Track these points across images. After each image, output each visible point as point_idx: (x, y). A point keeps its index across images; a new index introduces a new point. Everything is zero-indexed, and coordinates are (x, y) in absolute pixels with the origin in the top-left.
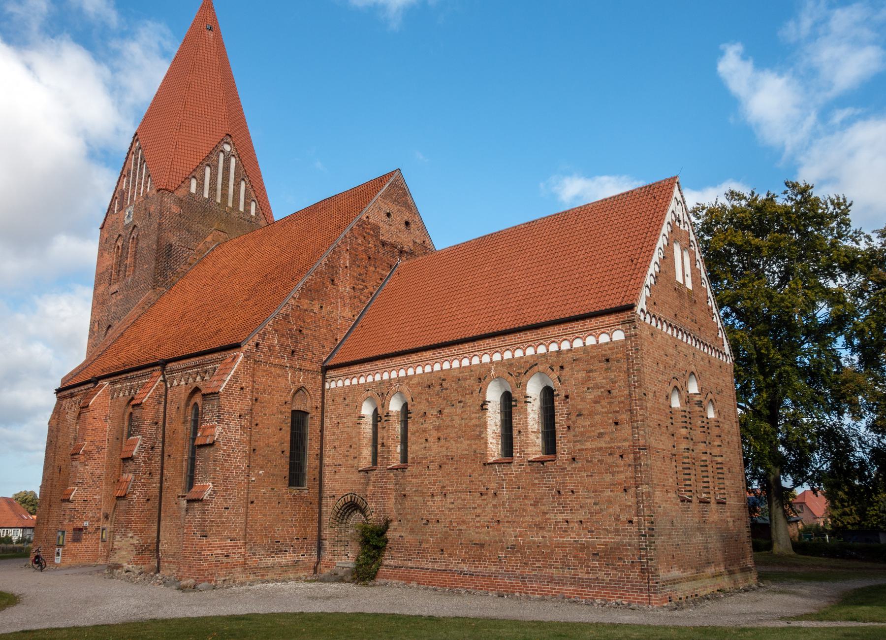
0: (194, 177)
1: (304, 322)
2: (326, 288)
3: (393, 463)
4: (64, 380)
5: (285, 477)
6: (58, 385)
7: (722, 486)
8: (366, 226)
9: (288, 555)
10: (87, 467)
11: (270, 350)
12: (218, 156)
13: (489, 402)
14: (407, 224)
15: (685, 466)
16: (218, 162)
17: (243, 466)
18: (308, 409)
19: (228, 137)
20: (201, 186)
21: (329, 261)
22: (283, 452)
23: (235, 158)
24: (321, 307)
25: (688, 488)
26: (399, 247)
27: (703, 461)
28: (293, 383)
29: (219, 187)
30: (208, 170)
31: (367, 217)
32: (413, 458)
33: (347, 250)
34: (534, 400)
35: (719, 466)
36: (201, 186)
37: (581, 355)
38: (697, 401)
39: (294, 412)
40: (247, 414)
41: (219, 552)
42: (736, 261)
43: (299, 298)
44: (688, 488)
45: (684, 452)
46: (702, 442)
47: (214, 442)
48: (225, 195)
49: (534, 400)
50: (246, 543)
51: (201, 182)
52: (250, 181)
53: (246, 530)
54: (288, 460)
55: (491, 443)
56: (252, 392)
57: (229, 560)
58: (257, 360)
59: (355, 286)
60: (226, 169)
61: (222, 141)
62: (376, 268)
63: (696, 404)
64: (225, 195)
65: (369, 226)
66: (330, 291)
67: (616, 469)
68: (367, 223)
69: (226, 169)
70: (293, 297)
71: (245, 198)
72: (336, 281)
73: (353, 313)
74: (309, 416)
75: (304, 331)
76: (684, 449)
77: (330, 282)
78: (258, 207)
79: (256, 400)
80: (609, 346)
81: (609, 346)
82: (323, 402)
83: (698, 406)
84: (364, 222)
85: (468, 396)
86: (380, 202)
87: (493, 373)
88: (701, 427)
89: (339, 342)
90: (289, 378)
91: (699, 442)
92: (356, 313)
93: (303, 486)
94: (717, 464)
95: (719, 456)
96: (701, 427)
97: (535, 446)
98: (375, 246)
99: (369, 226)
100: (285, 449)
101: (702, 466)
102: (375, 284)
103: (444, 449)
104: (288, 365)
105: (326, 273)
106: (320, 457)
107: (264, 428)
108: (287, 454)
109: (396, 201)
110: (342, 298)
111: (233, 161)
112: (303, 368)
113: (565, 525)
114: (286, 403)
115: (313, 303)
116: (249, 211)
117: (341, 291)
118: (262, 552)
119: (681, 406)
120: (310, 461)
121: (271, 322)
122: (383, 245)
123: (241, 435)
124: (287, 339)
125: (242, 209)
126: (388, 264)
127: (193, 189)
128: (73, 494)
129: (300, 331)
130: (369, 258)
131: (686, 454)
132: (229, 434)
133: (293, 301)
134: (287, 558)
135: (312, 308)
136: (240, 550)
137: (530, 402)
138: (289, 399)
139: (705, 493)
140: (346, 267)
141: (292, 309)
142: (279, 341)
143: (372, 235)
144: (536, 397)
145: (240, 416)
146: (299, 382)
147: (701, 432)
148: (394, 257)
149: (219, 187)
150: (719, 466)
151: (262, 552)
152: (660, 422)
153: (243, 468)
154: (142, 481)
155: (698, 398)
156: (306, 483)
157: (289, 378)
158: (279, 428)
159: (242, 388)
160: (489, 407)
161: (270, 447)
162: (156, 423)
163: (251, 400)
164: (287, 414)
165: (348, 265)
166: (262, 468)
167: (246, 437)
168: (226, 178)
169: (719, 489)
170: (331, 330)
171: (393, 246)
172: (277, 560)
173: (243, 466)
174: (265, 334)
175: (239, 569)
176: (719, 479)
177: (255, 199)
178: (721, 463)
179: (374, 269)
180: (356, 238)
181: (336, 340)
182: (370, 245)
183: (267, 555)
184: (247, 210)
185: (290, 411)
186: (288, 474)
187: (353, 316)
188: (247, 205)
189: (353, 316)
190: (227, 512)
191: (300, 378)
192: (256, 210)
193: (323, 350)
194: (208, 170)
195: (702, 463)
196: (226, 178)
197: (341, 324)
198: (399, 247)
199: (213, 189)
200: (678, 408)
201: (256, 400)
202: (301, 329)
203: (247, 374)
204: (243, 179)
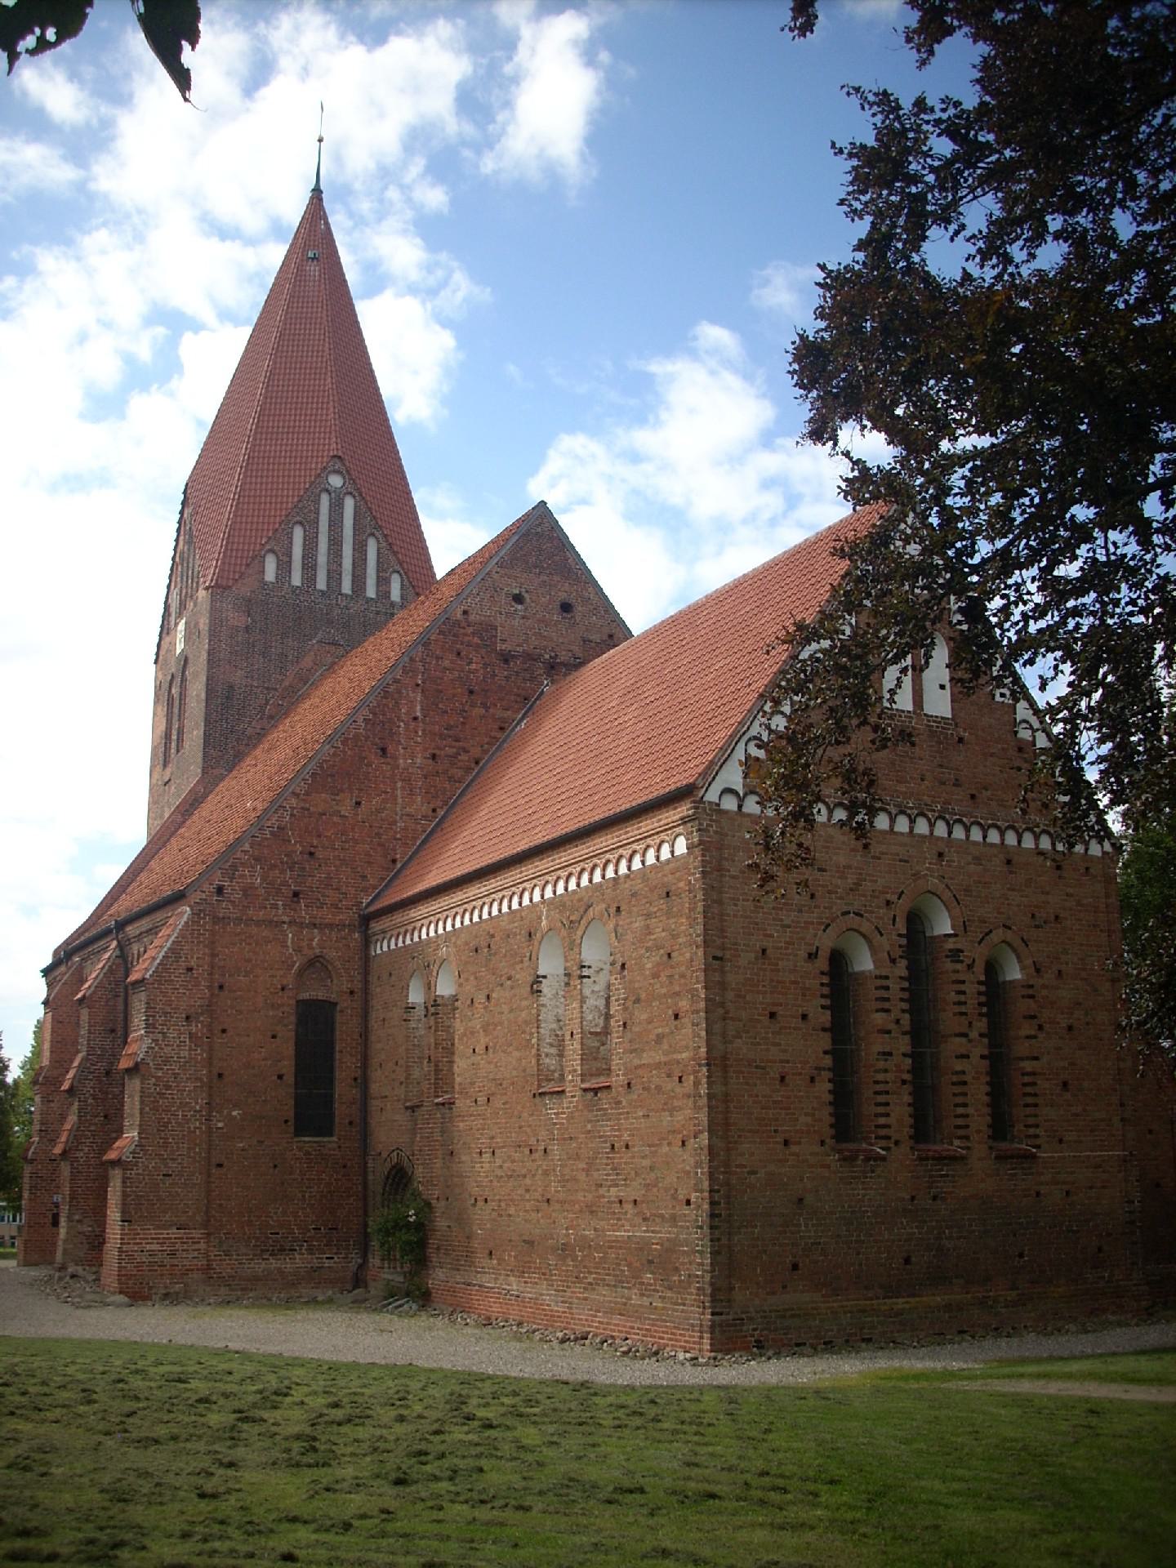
0: (272, 551)
1: (319, 836)
2: (369, 765)
3: (446, 1092)
4: (56, 952)
5: (286, 1121)
6: (48, 960)
7: (1031, 1121)
8: (462, 631)
9: (297, 1256)
10: (52, 1105)
11: (245, 895)
12: (317, 502)
13: (544, 977)
14: (566, 608)
15: (879, 1087)
16: (317, 512)
17: (197, 1103)
18: (333, 997)
19: (336, 460)
20: (284, 567)
21: (375, 714)
22: (280, 1077)
23: (354, 497)
24: (358, 804)
25: (882, 1132)
26: (547, 656)
27: (957, 1073)
28: (298, 950)
29: (322, 559)
30: (298, 534)
31: (465, 612)
32: (460, 1084)
33: (418, 685)
34: (598, 972)
35: (1026, 1079)
36: (284, 567)
37: (638, 885)
38: (950, 950)
39: (301, 1003)
40: (202, 1014)
41: (155, 1247)
42: (1147, 619)
43: (307, 794)
44: (882, 1132)
45: (877, 1060)
46: (957, 1035)
47: (137, 1065)
48: (334, 575)
49: (598, 972)
50: (209, 1234)
51: (286, 559)
52: (386, 536)
53: (207, 1212)
54: (292, 1090)
55: (547, 1055)
56: (211, 974)
57: (175, 1262)
58: (221, 915)
59: (437, 752)
60: (336, 524)
61: (326, 471)
62: (487, 709)
63: (947, 956)
64: (334, 575)
65: (470, 630)
66: (376, 770)
67: (676, 1103)
68: (463, 624)
69: (336, 524)
70: (293, 793)
71: (378, 571)
72: (390, 749)
73: (432, 806)
74: (338, 1008)
75: (319, 854)
76: (879, 1053)
77: (376, 753)
78: (405, 583)
79: (221, 987)
80: (671, 865)
81: (671, 865)
82: (366, 982)
83: (952, 961)
84: (458, 623)
85: (518, 967)
86: (496, 576)
87: (544, 923)
88: (955, 1004)
89: (399, 865)
90: (289, 943)
91: (951, 1036)
92: (439, 803)
93: (332, 1135)
94: (1023, 1074)
95: (1028, 1058)
96: (955, 1004)
97: (595, 1059)
98: (486, 665)
99: (470, 630)
100: (284, 1071)
101: (954, 1084)
102: (486, 740)
103: (492, 1066)
104: (286, 919)
105: (367, 738)
106: (363, 1081)
107: (238, 1035)
108: (290, 1078)
109: (535, 567)
110: (407, 780)
111: (349, 504)
112: (318, 921)
113: (616, 1208)
114: (283, 989)
115: (338, 798)
116: (387, 594)
117: (402, 766)
118: (244, 1251)
119: (876, 967)
120: (343, 1090)
121: (247, 845)
122: (506, 661)
123: (190, 1050)
124: (283, 872)
125: (371, 592)
126: (519, 695)
127: (270, 575)
128: (32, 1150)
129: (311, 854)
130: (471, 692)
131: (881, 1064)
132: (167, 1050)
133: (294, 801)
134: (299, 1261)
135: (336, 808)
136: (196, 1246)
137: (589, 977)
138: (290, 981)
139: (959, 1138)
140: (415, 719)
141: (292, 815)
142: (263, 879)
143: (478, 645)
144: (604, 967)
145: (188, 1018)
146: (310, 947)
147: (955, 1014)
148: (532, 679)
149: (322, 559)
150: (1026, 1079)
151: (244, 1251)
152: (774, 1009)
153: (198, 1108)
154: (93, 1128)
155: (950, 944)
156: (336, 1131)
157: (289, 943)
158: (270, 1034)
159: (190, 969)
160: (546, 987)
161: (253, 1068)
162: (113, 1031)
163: (210, 988)
164: (286, 1009)
165: (418, 714)
166: (236, 1106)
167: (201, 1054)
168: (335, 543)
169: (1026, 1126)
170: (380, 844)
171: (530, 657)
172: (274, 1264)
173: (197, 1103)
174: (234, 867)
175: (195, 1275)
176: (1026, 1105)
177: (397, 568)
178: (1033, 1074)
179: (483, 711)
180: (438, 658)
181: (394, 861)
182: (473, 666)
183: (255, 1255)
184: (384, 594)
185: (293, 1002)
186: (292, 1114)
187: (434, 810)
188: (383, 582)
189: (434, 810)
190: (169, 1181)
191: (312, 940)
192: (402, 589)
193: (364, 884)
194: (298, 534)
195: (955, 1079)
196: (335, 543)
197: (405, 829)
198: (547, 656)
199: (309, 566)
200: (870, 971)
201: (221, 987)
202: (312, 849)
203: (199, 942)
204: (373, 535)
